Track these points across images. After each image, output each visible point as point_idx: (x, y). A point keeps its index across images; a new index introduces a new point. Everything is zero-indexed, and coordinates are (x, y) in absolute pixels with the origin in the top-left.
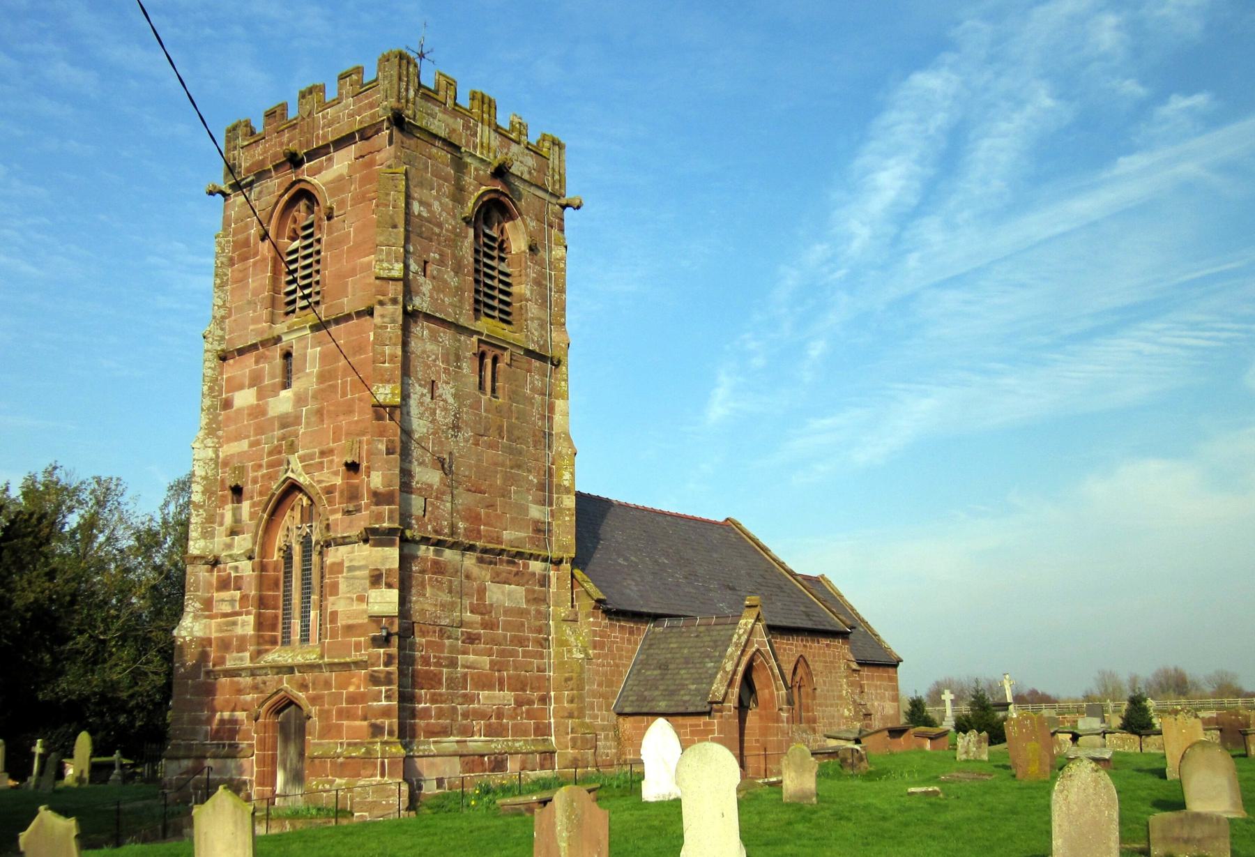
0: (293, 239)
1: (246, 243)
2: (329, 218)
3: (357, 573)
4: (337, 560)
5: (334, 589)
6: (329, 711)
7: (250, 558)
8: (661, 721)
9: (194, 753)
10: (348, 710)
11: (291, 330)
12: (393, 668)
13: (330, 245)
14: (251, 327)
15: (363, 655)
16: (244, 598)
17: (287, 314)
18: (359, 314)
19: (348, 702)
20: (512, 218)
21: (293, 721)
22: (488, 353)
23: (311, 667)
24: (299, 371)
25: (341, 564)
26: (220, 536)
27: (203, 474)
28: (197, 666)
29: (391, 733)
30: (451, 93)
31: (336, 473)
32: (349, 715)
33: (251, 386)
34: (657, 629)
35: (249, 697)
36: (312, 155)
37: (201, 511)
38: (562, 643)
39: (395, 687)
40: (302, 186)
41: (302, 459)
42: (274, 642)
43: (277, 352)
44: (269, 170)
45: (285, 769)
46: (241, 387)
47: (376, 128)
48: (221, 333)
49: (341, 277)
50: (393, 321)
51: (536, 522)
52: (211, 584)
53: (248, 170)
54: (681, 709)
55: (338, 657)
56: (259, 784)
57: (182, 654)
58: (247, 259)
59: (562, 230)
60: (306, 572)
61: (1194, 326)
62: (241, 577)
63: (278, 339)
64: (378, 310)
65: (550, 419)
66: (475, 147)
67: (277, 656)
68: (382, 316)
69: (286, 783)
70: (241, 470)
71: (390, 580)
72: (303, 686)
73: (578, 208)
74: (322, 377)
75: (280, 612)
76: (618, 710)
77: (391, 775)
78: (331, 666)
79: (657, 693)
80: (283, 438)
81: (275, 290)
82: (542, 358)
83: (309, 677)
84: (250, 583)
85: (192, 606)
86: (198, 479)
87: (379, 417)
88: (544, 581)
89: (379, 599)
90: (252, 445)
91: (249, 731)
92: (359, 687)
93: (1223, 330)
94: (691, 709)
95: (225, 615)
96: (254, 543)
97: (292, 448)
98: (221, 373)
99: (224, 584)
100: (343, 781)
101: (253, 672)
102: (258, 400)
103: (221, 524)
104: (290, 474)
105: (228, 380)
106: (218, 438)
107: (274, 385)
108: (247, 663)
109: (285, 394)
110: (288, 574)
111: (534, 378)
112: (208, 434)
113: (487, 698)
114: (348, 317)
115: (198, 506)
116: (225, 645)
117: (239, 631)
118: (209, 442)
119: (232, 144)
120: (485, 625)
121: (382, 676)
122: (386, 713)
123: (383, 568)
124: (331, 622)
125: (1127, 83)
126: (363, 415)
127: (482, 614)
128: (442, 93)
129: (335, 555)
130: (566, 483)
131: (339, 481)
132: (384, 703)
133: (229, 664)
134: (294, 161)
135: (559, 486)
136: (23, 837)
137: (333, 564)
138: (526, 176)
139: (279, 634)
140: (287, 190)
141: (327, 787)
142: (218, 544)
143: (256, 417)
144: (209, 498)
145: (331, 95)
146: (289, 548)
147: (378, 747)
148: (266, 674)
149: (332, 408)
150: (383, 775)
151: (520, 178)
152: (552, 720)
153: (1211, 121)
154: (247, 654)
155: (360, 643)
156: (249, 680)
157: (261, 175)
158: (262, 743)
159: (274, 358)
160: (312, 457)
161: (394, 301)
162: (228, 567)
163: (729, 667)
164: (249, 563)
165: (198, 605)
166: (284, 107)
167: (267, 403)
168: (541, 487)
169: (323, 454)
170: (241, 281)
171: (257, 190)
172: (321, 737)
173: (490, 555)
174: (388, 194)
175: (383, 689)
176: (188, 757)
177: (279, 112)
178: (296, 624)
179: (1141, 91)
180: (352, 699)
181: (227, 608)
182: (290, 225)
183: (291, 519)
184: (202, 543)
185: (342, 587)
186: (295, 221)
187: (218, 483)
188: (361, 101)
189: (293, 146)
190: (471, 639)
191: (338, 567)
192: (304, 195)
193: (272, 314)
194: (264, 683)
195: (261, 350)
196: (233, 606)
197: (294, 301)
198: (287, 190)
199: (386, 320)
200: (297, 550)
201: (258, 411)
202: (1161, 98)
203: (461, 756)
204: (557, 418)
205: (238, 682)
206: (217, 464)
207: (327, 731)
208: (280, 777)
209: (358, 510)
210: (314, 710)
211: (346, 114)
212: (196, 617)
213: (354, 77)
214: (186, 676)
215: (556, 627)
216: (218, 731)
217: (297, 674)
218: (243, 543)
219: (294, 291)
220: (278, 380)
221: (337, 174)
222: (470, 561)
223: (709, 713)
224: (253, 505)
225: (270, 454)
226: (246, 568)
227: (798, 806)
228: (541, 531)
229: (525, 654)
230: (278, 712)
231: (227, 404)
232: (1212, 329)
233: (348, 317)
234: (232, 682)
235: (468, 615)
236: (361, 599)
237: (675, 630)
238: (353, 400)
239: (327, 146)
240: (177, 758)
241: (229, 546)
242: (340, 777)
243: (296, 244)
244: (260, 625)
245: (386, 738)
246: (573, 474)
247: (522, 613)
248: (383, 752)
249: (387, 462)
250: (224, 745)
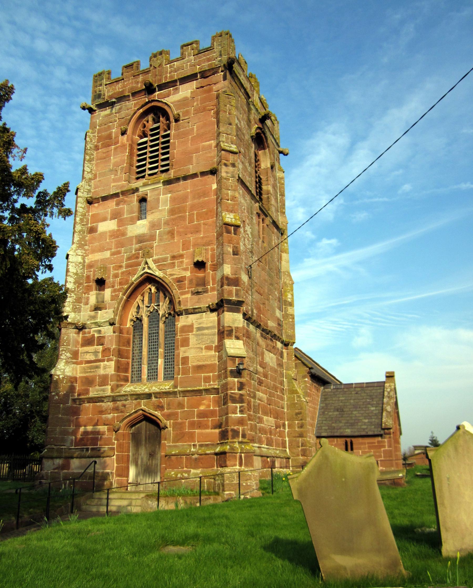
1: (109, 137)
3: (206, 331)
4: (189, 323)
5: (186, 342)
6: (182, 424)
7: (112, 324)
9: (64, 455)
10: (199, 423)
11: (145, 185)
13: (177, 136)
14: (113, 184)
17: (138, 178)
19: (199, 416)
20: (264, 148)
21: (143, 432)
23: (167, 394)
24: (152, 208)
25: (192, 326)
26: (85, 311)
27: (75, 271)
28: (67, 395)
31: (186, 269)
32: (200, 426)
33: (112, 219)
34: (326, 390)
35: (110, 416)
36: (161, 87)
37: (73, 295)
38: (293, 392)
41: (155, 261)
42: (126, 380)
43: (135, 198)
44: (129, 96)
45: (137, 465)
46: (104, 219)
47: (214, 71)
48: (89, 188)
52: (78, 342)
55: (190, 387)
56: (118, 475)
57: (57, 387)
58: (109, 146)
61: (334, 323)
62: (104, 337)
63: (137, 190)
67: (129, 388)
68: (227, 172)
69: (137, 475)
71: (238, 334)
72: (160, 407)
73: (287, 155)
74: (172, 212)
75: (130, 360)
76: (318, 435)
78: (185, 393)
79: (341, 425)
80: (140, 249)
83: (164, 401)
84: (111, 341)
85: (64, 355)
86: (71, 274)
89: (232, 346)
90: (112, 254)
91: (111, 439)
92: (209, 406)
93: (344, 325)
94: (370, 433)
96: (116, 315)
97: (148, 254)
98: (88, 212)
99: (88, 342)
100: (199, 471)
101: (114, 399)
102: (119, 226)
103: (87, 304)
105: (93, 216)
106: (85, 250)
107: (132, 217)
108: (109, 393)
112: (79, 247)
114: (194, 176)
116: (89, 382)
117: (102, 372)
118: (79, 252)
119: (99, 83)
121: (237, 396)
124: (183, 364)
125: (308, 233)
130: (289, 300)
131: (188, 274)
132: (239, 415)
133: (92, 394)
134: (149, 89)
135: (286, 301)
137: (184, 327)
139: (129, 375)
140: (143, 106)
141: (186, 475)
143: (118, 237)
144: (78, 287)
145: (175, 54)
146: (140, 320)
147: (237, 445)
148: (126, 400)
149: (181, 230)
150: (241, 465)
151: (268, 128)
152: (287, 439)
153: (338, 251)
154: (109, 387)
155: (209, 377)
156: (111, 404)
157: (122, 98)
158: (120, 446)
159: (132, 202)
160: (165, 259)
162: (93, 331)
164: (111, 328)
165: (68, 355)
167: (126, 229)
170: (106, 158)
171: (118, 107)
174: (226, 106)
175: (238, 405)
176: (60, 458)
177: (135, 65)
178: (145, 368)
179: (313, 237)
181: (91, 357)
186: (144, 126)
187: (85, 278)
188: (201, 58)
191: (188, 328)
194: (124, 406)
195: (121, 197)
196: (96, 356)
197: (144, 171)
198: (143, 106)
199: (229, 175)
201: (118, 234)
202: (319, 239)
203: (262, 456)
204: (283, 263)
205: (101, 406)
206: (84, 266)
207: (180, 437)
208: (132, 472)
209: (206, 291)
211: (191, 64)
212: (67, 363)
213: (194, 45)
214: (59, 402)
215: (288, 382)
216: (81, 439)
217: (154, 399)
219: (145, 165)
220: (136, 214)
221: (182, 97)
223: (381, 436)
225: (129, 259)
230: (132, 426)
231: (92, 230)
232: (340, 324)
233: (194, 176)
234: (94, 407)
237: (339, 390)
238: (199, 224)
239: (175, 81)
240: (52, 458)
241: (94, 317)
242: (194, 468)
244: (118, 368)
245: (240, 439)
246: (292, 295)
248: (242, 449)
249: (234, 259)
250: (87, 449)
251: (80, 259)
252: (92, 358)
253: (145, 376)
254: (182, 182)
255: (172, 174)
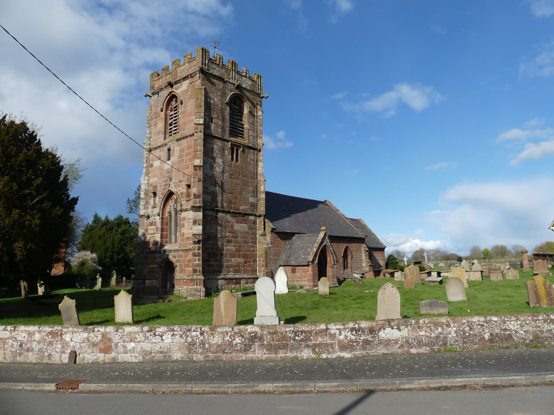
0: (171, 111)
2: (182, 104)
5: (183, 225)
8: (281, 268)
12: (200, 251)
15: (191, 247)
16: (157, 228)
18: (190, 136)
22: (235, 147)
23: (176, 251)
29: (200, 272)
30: (221, 61)
31: (184, 188)
32: (188, 266)
36: (176, 83)
39: (201, 257)
40: (173, 93)
49: (184, 123)
50: (200, 138)
51: (252, 203)
53: (157, 88)
54: (299, 264)
59: (261, 106)
60: (176, 220)
63: (166, 145)
64: (195, 134)
65: (257, 169)
66: (230, 79)
70: (155, 187)
74: (180, 157)
77: (200, 285)
81: (166, 128)
82: (254, 149)
83: (176, 254)
87: (196, 170)
88: (255, 222)
94: (302, 264)
95: (152, 234)
99: (151, 224)
104: (170, 188)
109: (169, 162)
110: (171, 220)
111: (251, 155)
113: (234, 261)
114: (187, 137)
115: (142, 199)
118: (146, 178)
120: (233, 237)
122: (198, 265)
123: (197, 219)
126: (191, 170)
127: (232, 233)
128: (218, 61)
129: (184, 214)
134: (171, 85)
136: (60, 305)
138: (248, 88)
139: (168, 240)
142: (149, 211)
145: (182, 63)
146: (171, 212)
157: (161, 89)
161: (201, 131)
163: (315, 250)
166: (168, 67)
168: (253, 192)
169: (180, 182)
172: (180, 273)
173: (236, 214)
178: (173, 237)
180: (189, 261)
182: (170, 107)
183: (171, 203)
184: (144, 211)
185: (186, 225)
189: (170, 80)
190: (229, 242)
191: (184, 219)
192: (172, 97)
193: (165, 136)
198: (169, 95)
200: (173, 212)
201: (161, 169)
209: (190, 200)
210: (178, 264)
211: (185, 69)
218: (157, 210)
219: (171, 128)
222: (228, 217)
224: (160, 198)
226: (158, 219)
227: (324, 297)
228: (254, 206)
229: (248, 246)
231: (152, 166)
233: (187, 137)
235: (228, 234)
236: (191, 229)
239: (180, 80)
241: (153, 212)
243: (172, 113)
247: (246, 233)
251: (147, 182)
252: (152, 232)
253: (173, 240)
254: (183, 140)
255: (178, 136)
